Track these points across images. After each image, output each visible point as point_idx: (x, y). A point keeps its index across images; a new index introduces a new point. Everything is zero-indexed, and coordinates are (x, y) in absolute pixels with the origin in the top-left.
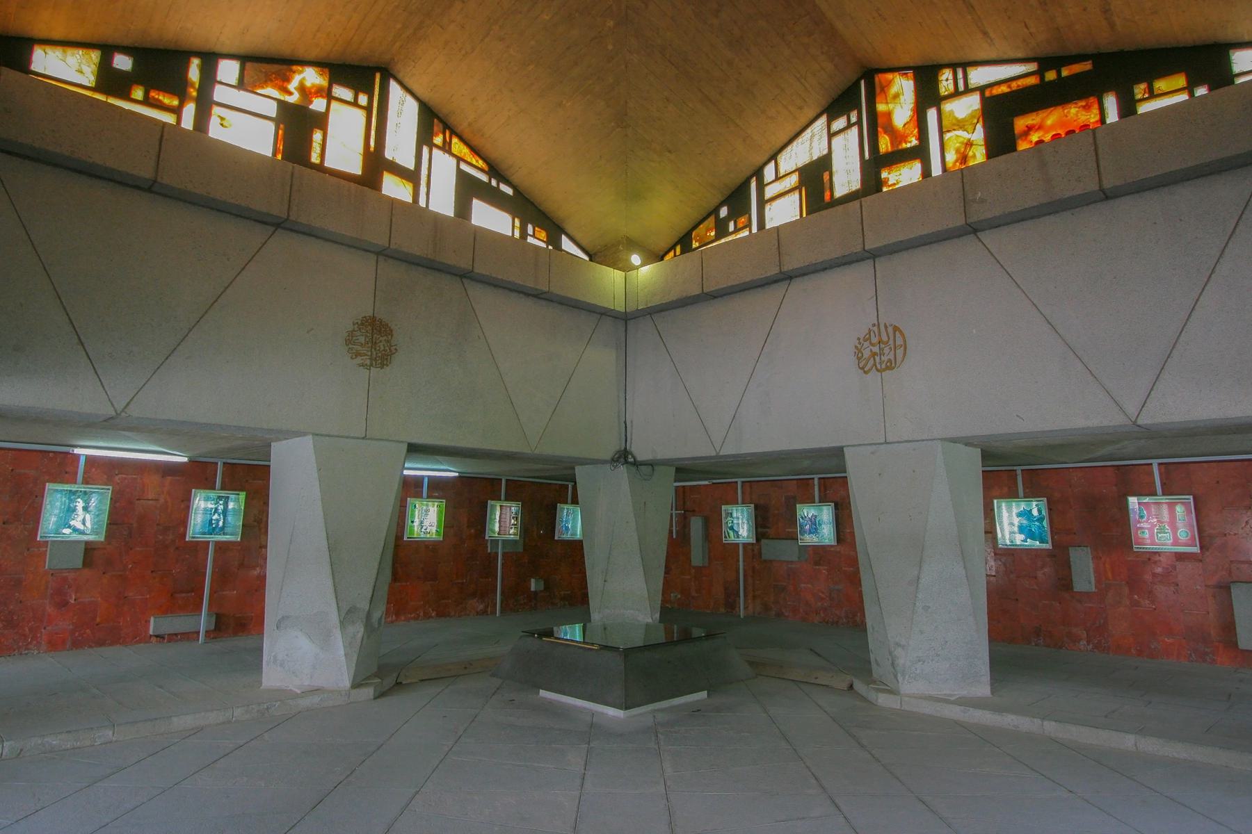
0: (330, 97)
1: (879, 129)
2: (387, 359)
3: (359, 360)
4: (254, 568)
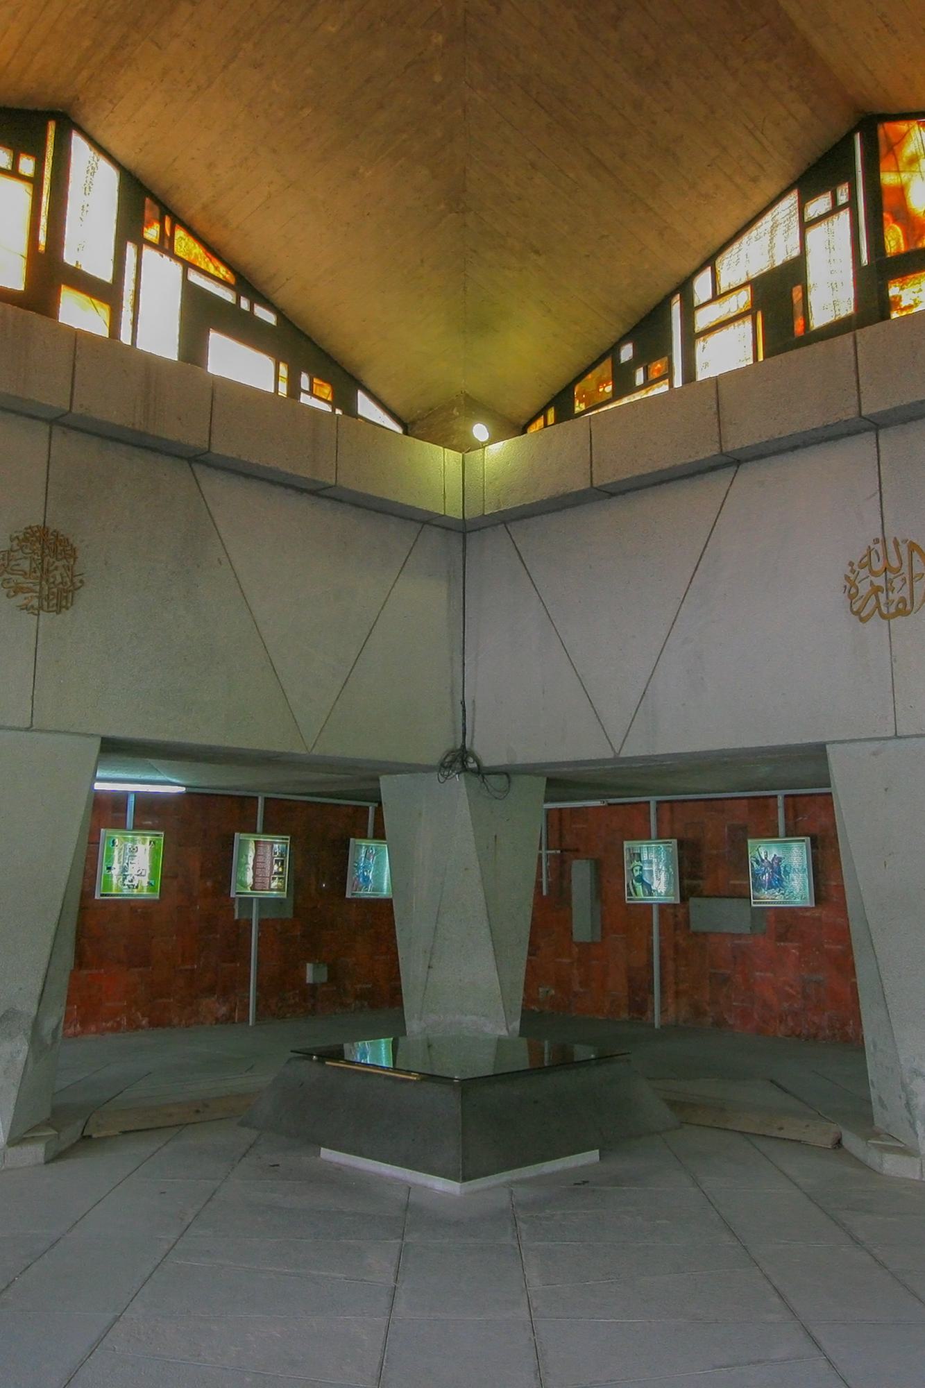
2: (66, 597)
3: (20, 599)
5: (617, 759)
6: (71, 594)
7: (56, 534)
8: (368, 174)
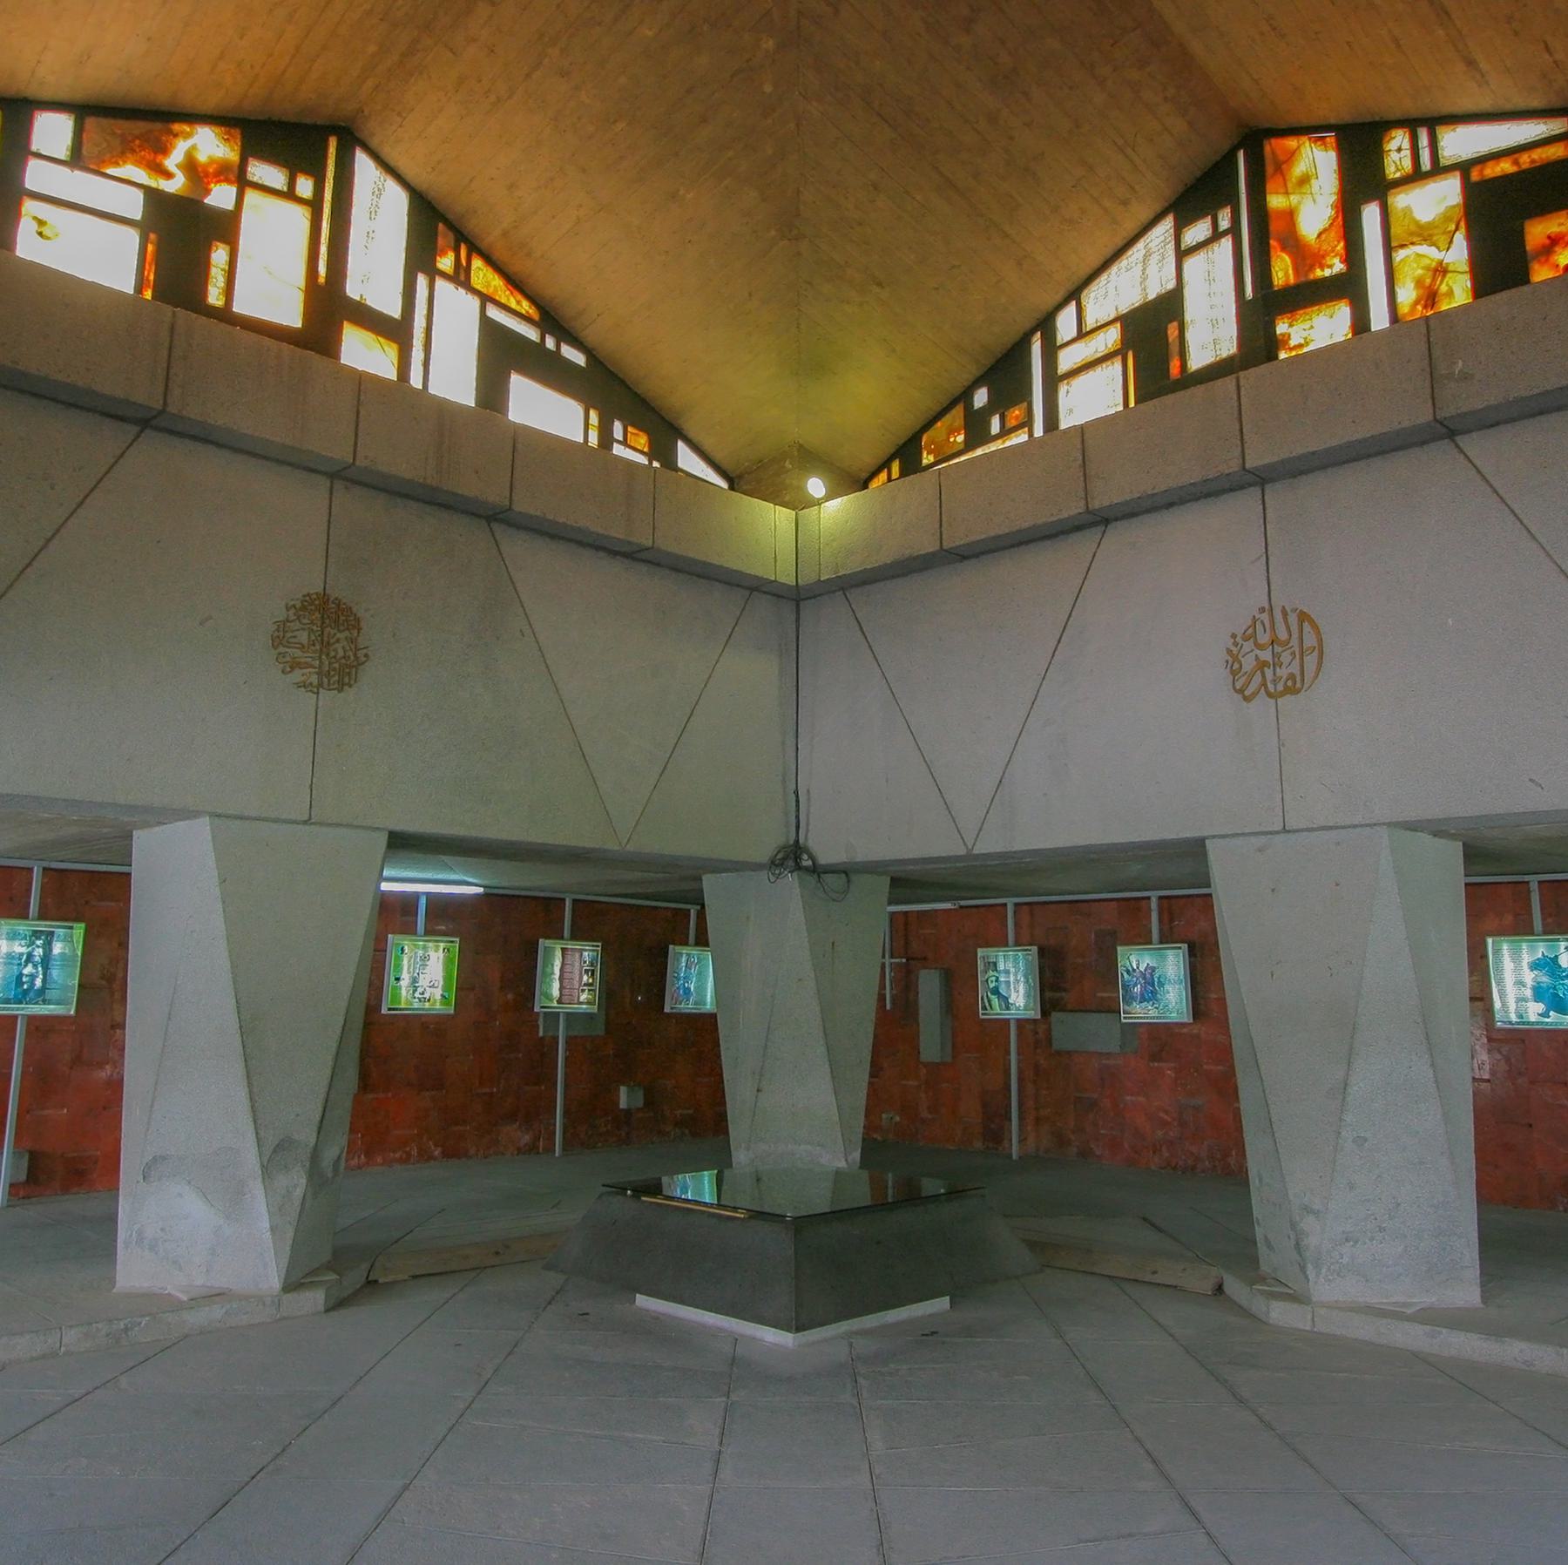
1: (1273, 243)
2: (349, 674)
3: (297, 676)
5: (970, 856)
6: (354, 669)
7: (338, 602)
8: (689, 196)
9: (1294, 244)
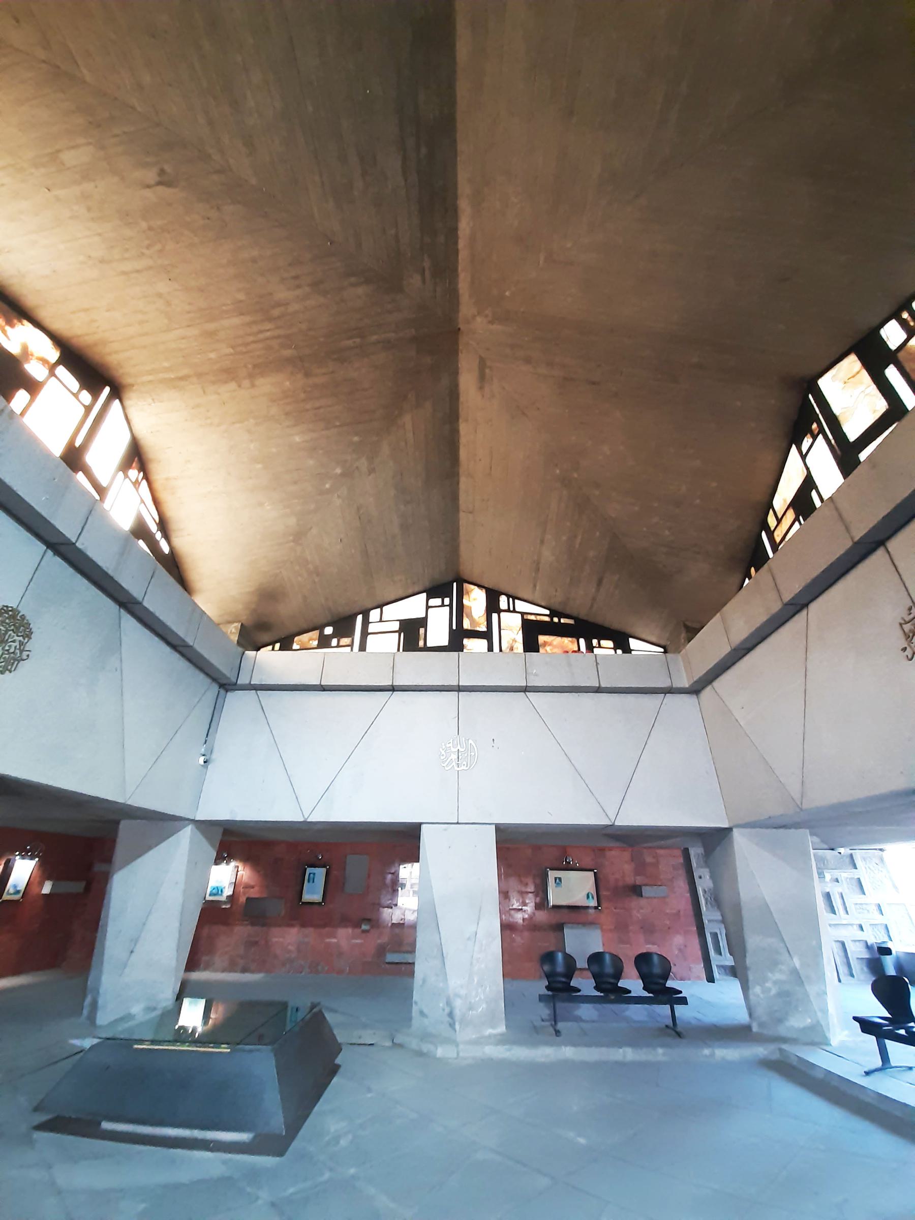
0: (52, 373)
1: (464, 615)
2: (13, 664)
4: (388, 924)
5: (305, 823)
6: (16, 663)
7: (23, 617)
8: (268, 508)
9: (470, 617)
